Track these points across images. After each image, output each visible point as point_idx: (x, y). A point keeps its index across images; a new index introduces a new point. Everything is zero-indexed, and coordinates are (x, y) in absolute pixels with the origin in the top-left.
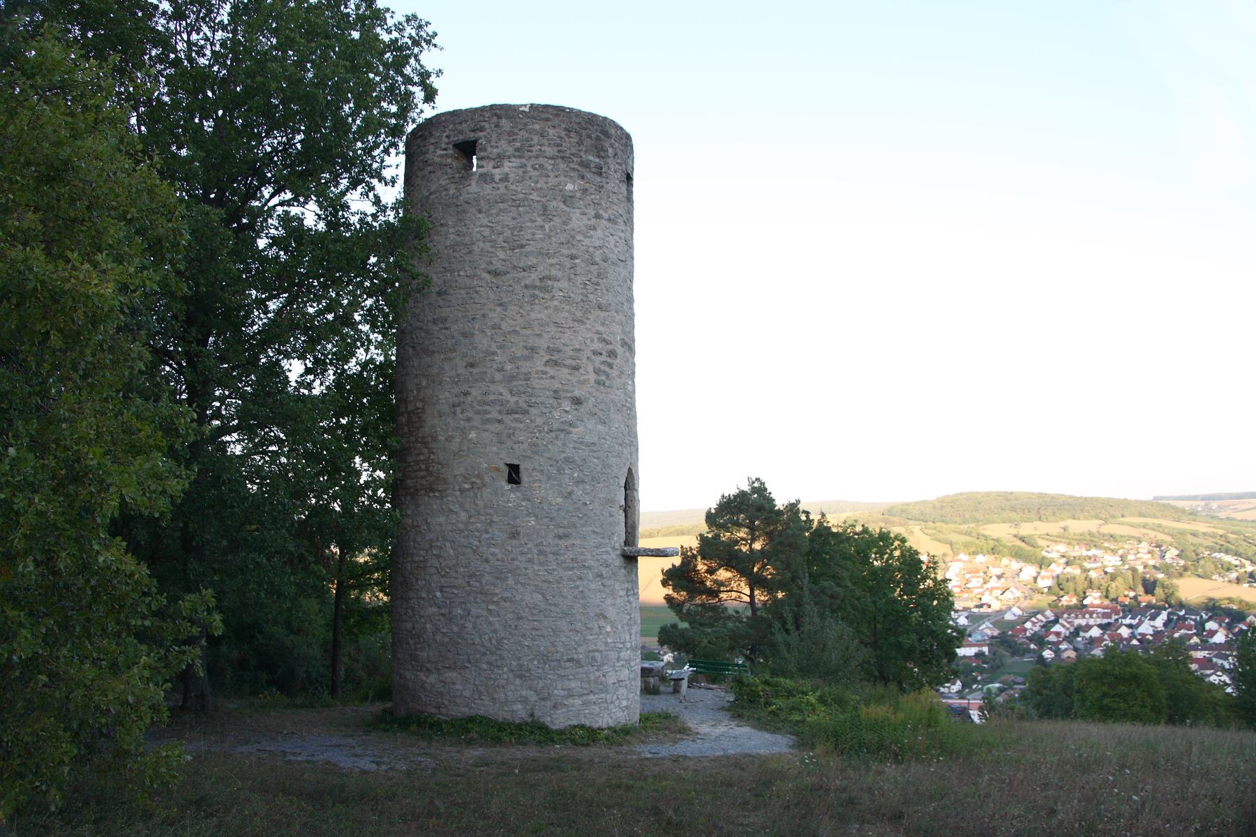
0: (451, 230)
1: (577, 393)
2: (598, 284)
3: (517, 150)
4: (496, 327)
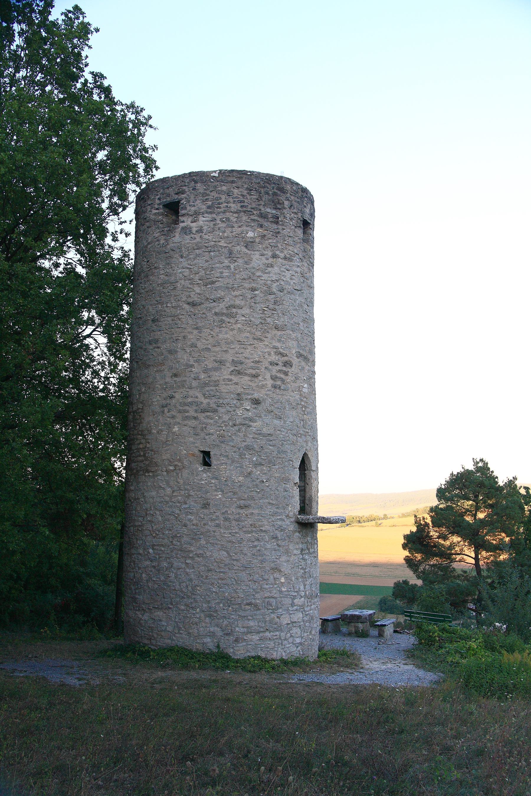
0: (162, 272)
1: (256, 396)
2: (274, 310)
3: (209, 207)
4: (194, 346)
